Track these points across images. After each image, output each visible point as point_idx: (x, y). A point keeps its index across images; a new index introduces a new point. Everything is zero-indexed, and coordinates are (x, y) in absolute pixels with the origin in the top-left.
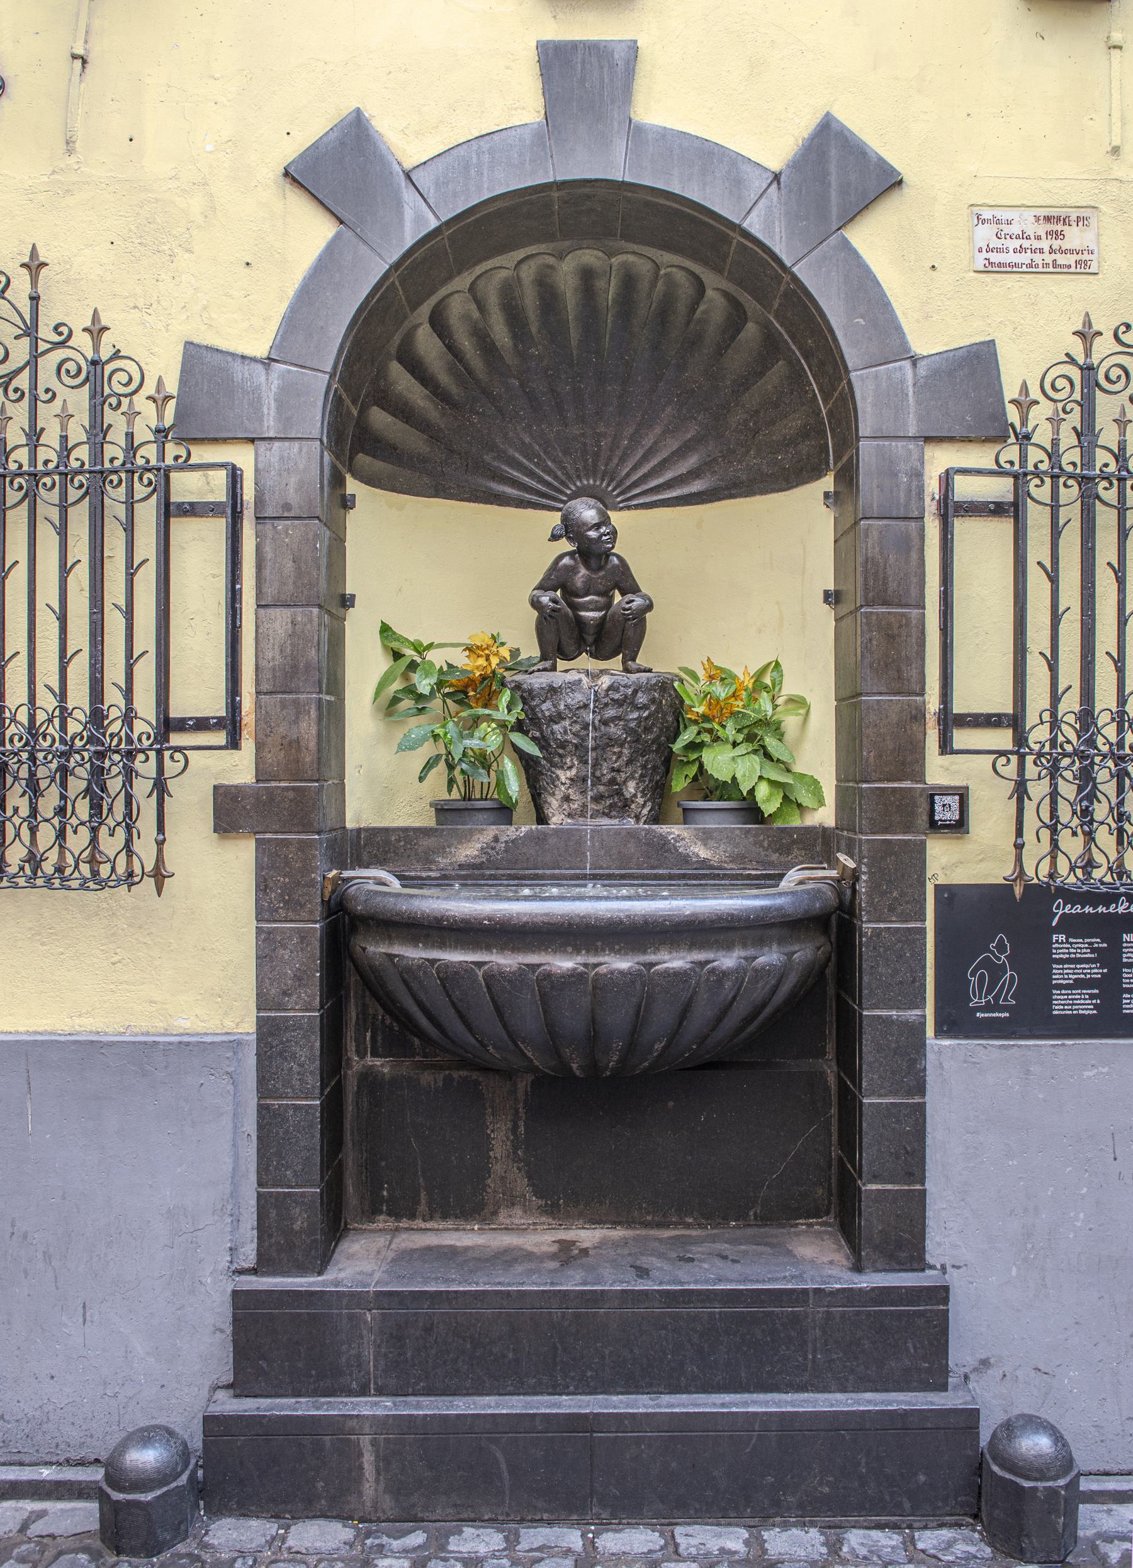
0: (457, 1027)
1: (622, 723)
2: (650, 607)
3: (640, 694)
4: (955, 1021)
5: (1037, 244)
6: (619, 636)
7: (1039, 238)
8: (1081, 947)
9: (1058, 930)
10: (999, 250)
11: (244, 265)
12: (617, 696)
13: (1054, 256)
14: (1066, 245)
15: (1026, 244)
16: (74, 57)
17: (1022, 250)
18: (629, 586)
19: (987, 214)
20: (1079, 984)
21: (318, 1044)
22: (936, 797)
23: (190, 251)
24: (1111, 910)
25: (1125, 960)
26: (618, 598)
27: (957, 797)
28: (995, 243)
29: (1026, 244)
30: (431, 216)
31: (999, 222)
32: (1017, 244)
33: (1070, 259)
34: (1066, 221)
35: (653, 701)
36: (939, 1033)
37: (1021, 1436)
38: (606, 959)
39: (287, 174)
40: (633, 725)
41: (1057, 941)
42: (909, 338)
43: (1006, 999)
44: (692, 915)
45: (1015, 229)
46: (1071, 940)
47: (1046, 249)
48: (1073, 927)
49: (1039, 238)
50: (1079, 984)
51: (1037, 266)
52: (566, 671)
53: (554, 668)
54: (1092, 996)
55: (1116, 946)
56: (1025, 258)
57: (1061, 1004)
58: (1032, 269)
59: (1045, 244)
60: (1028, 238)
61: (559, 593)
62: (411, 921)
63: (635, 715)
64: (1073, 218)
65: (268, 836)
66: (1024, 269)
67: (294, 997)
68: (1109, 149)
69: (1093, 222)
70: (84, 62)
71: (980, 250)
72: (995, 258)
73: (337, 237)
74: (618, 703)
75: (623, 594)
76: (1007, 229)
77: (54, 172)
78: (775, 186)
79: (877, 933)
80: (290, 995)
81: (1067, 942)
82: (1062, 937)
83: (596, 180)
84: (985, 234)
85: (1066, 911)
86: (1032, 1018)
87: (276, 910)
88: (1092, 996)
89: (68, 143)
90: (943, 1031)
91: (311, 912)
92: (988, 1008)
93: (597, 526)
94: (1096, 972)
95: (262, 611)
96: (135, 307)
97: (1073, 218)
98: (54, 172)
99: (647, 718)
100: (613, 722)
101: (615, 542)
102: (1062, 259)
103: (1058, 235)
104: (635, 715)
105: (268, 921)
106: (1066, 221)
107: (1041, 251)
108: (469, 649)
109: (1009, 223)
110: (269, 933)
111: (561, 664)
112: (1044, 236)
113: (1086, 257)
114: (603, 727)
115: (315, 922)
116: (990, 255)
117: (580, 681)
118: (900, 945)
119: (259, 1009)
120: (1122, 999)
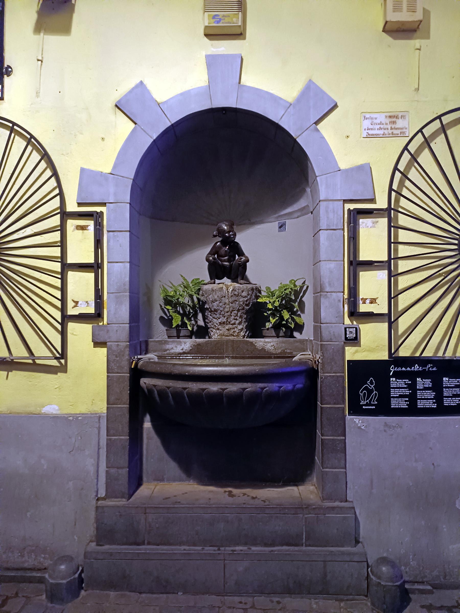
2: (248, 261)
4: (356, 409)
5: (386, 127)
6: (237, 272)
7: (387, 124)
8: (401, 383)
9: (392, 376)
10: (372, 129)
11: (100, 140)
13: (392, 131)
14: (397, 126)
15: (382, 126)
16: (38, 60)
17: (380, 129)
18: (241, 253)
19: (368, 116)
20: (401, 396)
22: (347, 329)
23: (82, 134)
24: (412, 369)
25: (418, 388)
26: (237, 257)
27: (355, 329)
28: (371, 127)
29: (382, 126)
30: (168, 121)
31: (372, 119)
32: (378, 126)
33: (398, 132)
34: (397, 117)
36: (350, 414)
38: (230, 387)
41: (392, 381)
42: (338, 163)
43: (373, 402)
45: (378, 121)
46: (397, 380)
47: (389, 128)
48: (398, 375)
49: (387, 124)
50: (401, 396)
51: (386, 135)
52: (219, 284)
53: (214, 283)
54: (406, 401)
55: (414, 383)
56: (381, 132)
57: (394, 404)
58: (384, 136)
59: (389, 126)
60: (383, 124)
61: (216, 256)
64: (400, 116)
66: (381, 136)
68: (414, 89)
69: (407, 117)
70: (42, 62)
71: (365, 130)
72: (371, 132)
73: (135, 129)
75: (239, 256)
76: (375, 121)
77: (32, 104)
81: (396, 381)
82: (394, 379)
83: (51, 365)
84: (367, 123)
85: (395, 369)
86: (384, 408)
88: (406, 401)
89: (37, 93)
90: (351, 413)
92: (367, 405)
93: (229, 232)
94: (407, 392)
95: (109, 264)
96: (63, 154)
97: (400, 116)
98: (32, 104)
99: (246, 301)
102: (395, 132)
103: (394, 123)
106: (397, 117)
107: (388, 129)
109: (376, 119)
111: (217, 281)
112: (389, 123)
113: (404, 130)
116: (368, 131)
117: (222, 287)
120: (417, 402)
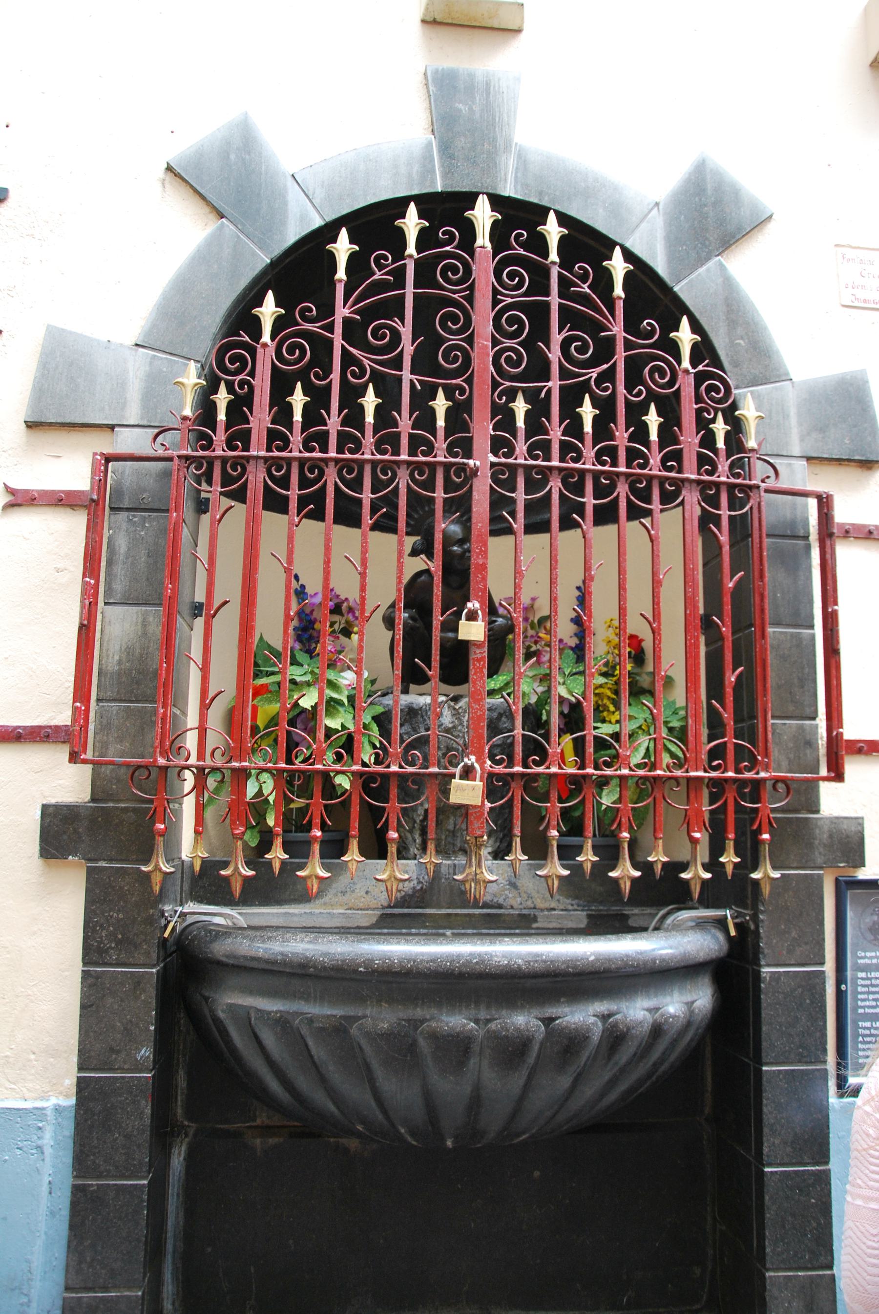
0: (304, 1083)
3: (504, 719)
21: (148, 1111)
39: (31, 425)
62: (507, 973)
65: (103, 864)
67: (123, 1055)
78: (656, 208)
79: (775, 976)
80: (118, 1052)
87: (106, 951)
91: (148, 954)
101: (486, 552)
105: (97, 964)
110: (97, 978)
115: (153, 966)
116: (855, 291)
118: (800, 990)
119: (80, 1069)
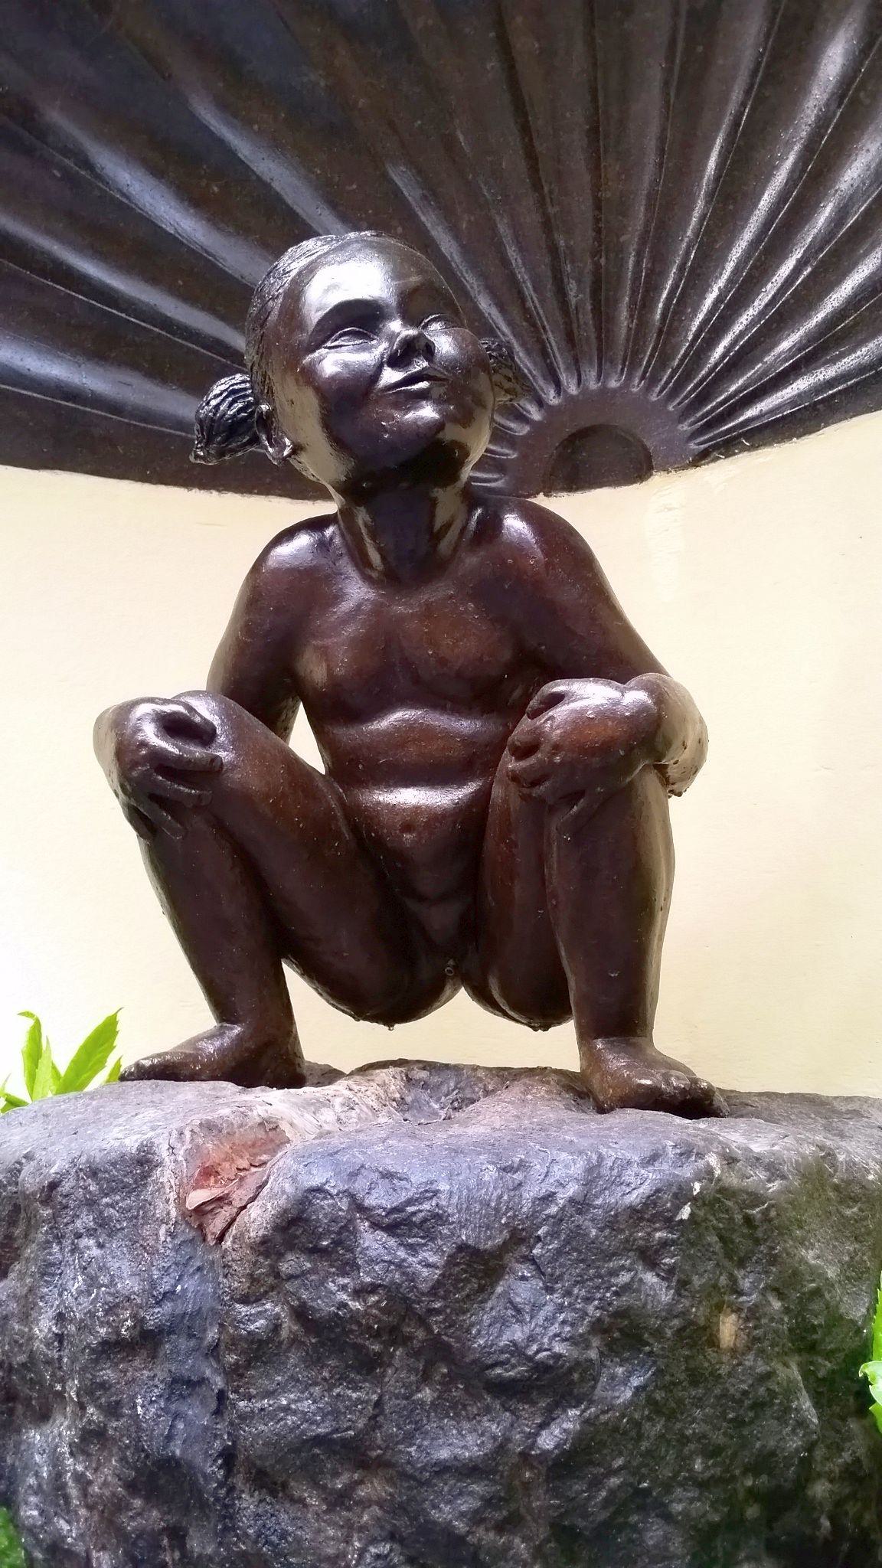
1: (373, 1488)
3: (521, 1286)
12: (337, 1294)
35: (623, 1332)
37: (315, 689)
40: (452, 1510)
44: (676, 684)
63: (460, 1442)
74: (327, 1338)
100: (313, 1475)
104: (460, 1442)
108: (520, 1185)
114: (248, 1503)
